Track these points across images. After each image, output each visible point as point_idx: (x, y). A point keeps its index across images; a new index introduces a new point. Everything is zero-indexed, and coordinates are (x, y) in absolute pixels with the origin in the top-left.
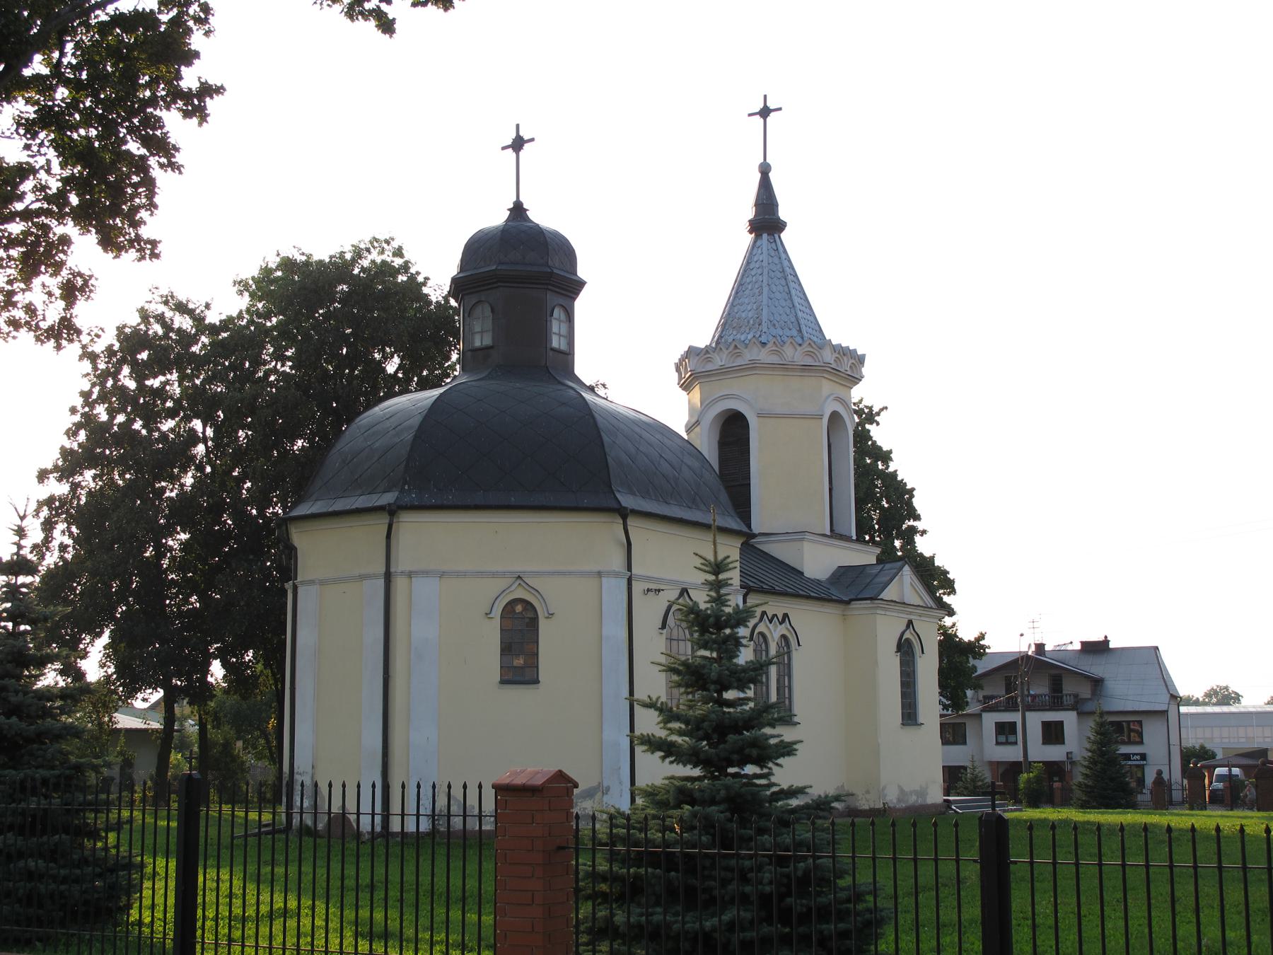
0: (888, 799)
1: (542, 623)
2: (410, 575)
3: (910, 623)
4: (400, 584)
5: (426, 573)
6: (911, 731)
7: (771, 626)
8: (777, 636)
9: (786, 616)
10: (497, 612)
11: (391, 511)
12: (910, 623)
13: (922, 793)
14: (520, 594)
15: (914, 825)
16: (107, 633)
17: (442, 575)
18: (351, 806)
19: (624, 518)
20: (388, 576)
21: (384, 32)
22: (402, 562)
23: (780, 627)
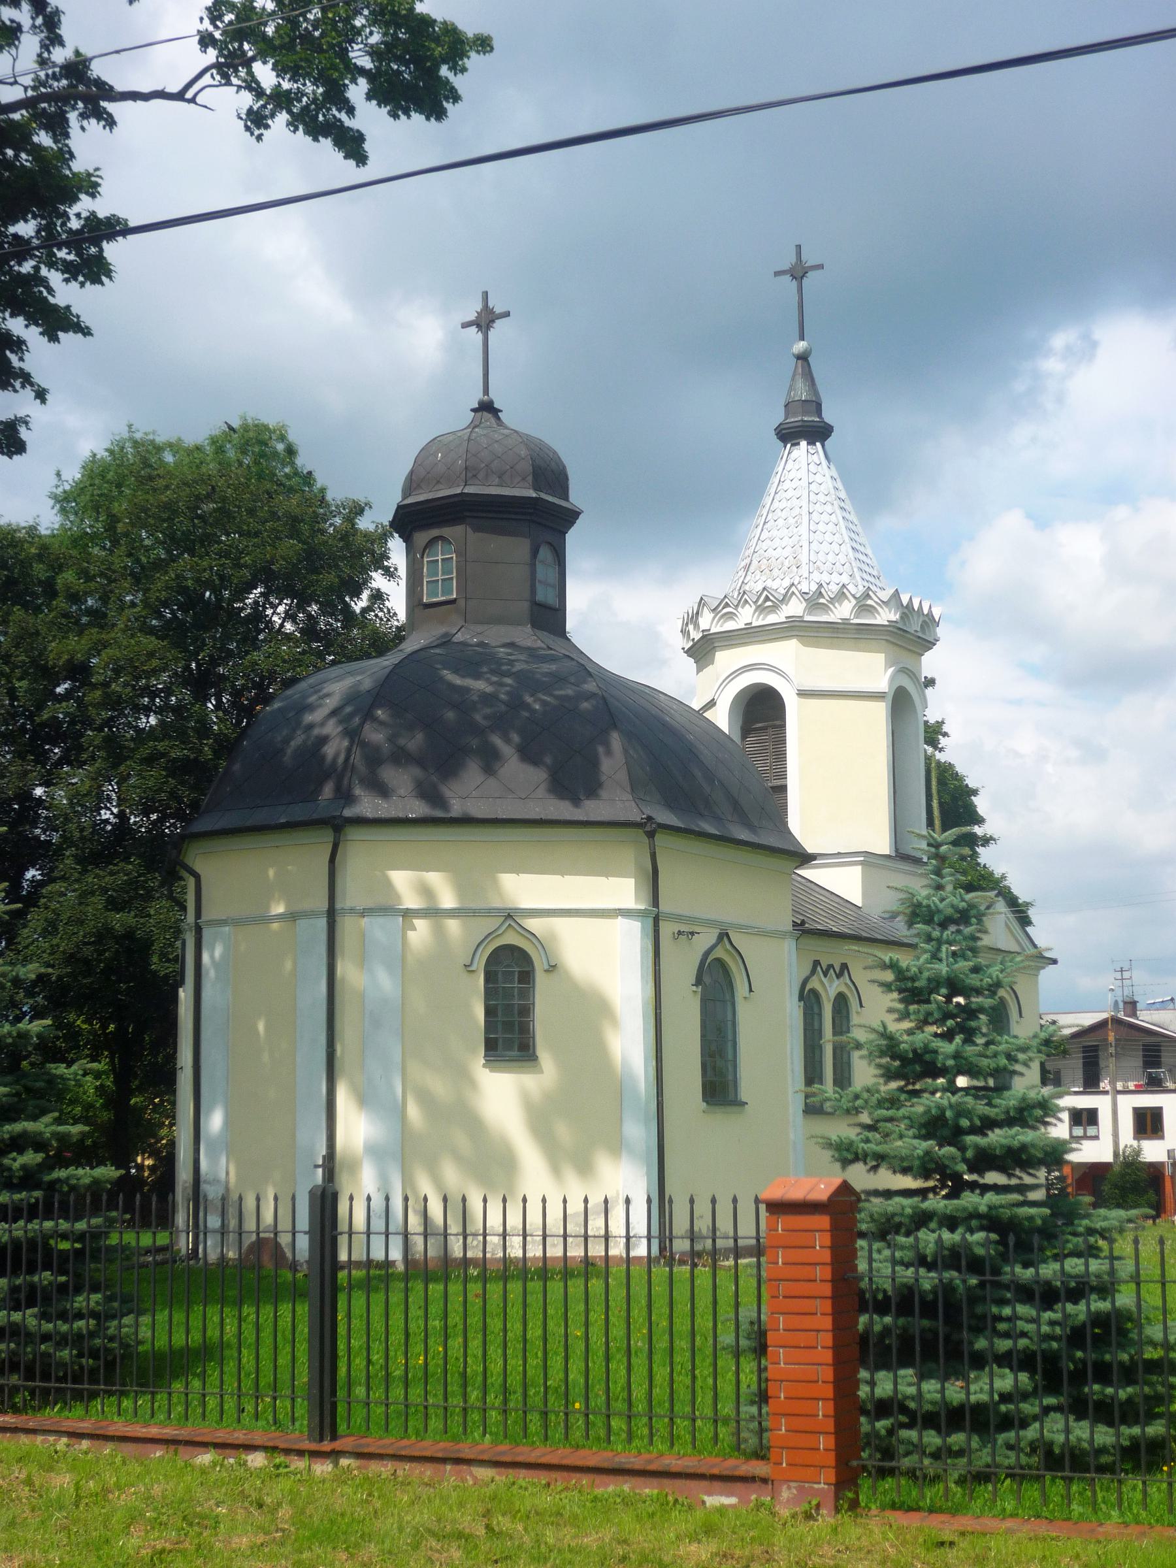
1: (540, 978)
8: (832, 993)
9: (844, 967)
10: (480, 964)
14: (511, 939)
15: (496, 1562)
16: (12, 230)
18: (284, 1224)
19: (651, 835)
20: (332, 915)
23: (836, 982)
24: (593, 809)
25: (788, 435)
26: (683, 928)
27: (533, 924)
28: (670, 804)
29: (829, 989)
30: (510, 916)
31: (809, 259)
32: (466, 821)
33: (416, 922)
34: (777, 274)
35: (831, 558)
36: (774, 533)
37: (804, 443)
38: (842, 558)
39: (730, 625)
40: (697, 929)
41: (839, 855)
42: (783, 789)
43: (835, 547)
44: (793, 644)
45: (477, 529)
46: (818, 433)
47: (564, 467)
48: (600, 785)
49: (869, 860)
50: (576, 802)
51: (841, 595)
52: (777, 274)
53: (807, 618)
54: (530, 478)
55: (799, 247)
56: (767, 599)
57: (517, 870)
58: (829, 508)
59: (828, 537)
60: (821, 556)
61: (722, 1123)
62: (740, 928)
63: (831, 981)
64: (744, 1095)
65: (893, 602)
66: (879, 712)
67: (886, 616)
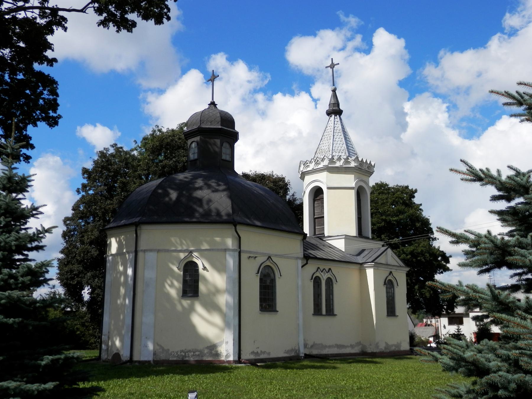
0: (380, 347)
2: (144, 251)
3: (391, 273)
4: (140, 255)
5: (151, 250)
6: (391, 320)
7: (322, 274)
9: (330, 269)
11: (137, 225)
12: (391, 273)
13: (399, 345)
17: (159, 251)
19: (235, 226)
21: (404, 197)
22: (142, 245)
23: (327, 274)
25: (329, 113)
26: (252, 255)
29: (324, 277)
31: (335, 62)
35: (339, 148)
36: (324, 142)
37: (333, 116)
38: (343, 148)
39: (309, 169)
40: (256, 256)
42: (323, 217)
43: (341, 145)
47: (234, 120)
49: (347, 238)
51: (339, 159)
53: (329, 166)
58: (340, 134)
62: (276, 256)
63: (325, 274)
66: (352, 194)
67: (353, 164)
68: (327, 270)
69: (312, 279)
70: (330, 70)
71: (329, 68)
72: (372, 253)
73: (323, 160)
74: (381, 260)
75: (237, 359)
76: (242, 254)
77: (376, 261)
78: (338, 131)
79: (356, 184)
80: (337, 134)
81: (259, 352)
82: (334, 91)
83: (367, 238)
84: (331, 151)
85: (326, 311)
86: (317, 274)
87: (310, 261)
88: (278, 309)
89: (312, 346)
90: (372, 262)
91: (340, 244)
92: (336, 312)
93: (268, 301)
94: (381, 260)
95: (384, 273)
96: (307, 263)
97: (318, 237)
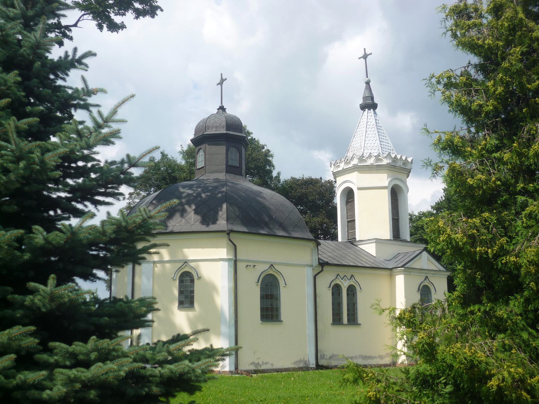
1: (196, 281)
3: (427, 277)
7: (342, 281)
9: (352, 276)
12: (427, 277)
24: (212, 227)
25: (363, 107)
27: (192, 264)
28: (245, 224)
29: (345, 285)
30: (186, 262)
31: (368, 52)
32: (172, 233)
33: (158, 265)
34: (359, 58)
35: (372, 145)
36: (357, 139)
37: (367, 110)
38: (376, 145)
39: (339, 169)
41: (369, 240)
42: (354, 221)
43: (374, 141)
44: (356, 173)
45: (209, 145)
46: (374, 106)
48: (217, 220)
49: (378, 241)
50: (208, 225)
51: (370, 156)
52: (359, 58)
54: (225, 128)
55: (365, 49)
56: (348, 160)
57: (189, 247)
58: (373, 129)
59: (372, 138)
60: (369, 145)
61: (271, 328)
62: (276, 263)
64: (282, 319)
65: (388, 157)
67: (385, 162)
68: (349, 278)
69: (330, 287)
70: (363, 60)
71: (362, 59)
72: (406, 257)
73: (352, 159)
74: (415, 264)
75: (233, 369)
76: (239, 264)
77: (407, 266)
78: (371, 126)
79: (390, 183)
80: (370, 130)
81: (261, 363)
82: (368, 83)
83: (406, 241)
84: (363, 149)
85: (349, 320)
86: (338, 282)
87: (326, 268)
88: (282, 318)
89: (331, 358)
90: (402, 266)
91: (371, 249)
92: (360, 320)
93: (270, 311)
94: (415, 264)
95: (418, 280)
96: (322, 270)
97: (350, 242)
